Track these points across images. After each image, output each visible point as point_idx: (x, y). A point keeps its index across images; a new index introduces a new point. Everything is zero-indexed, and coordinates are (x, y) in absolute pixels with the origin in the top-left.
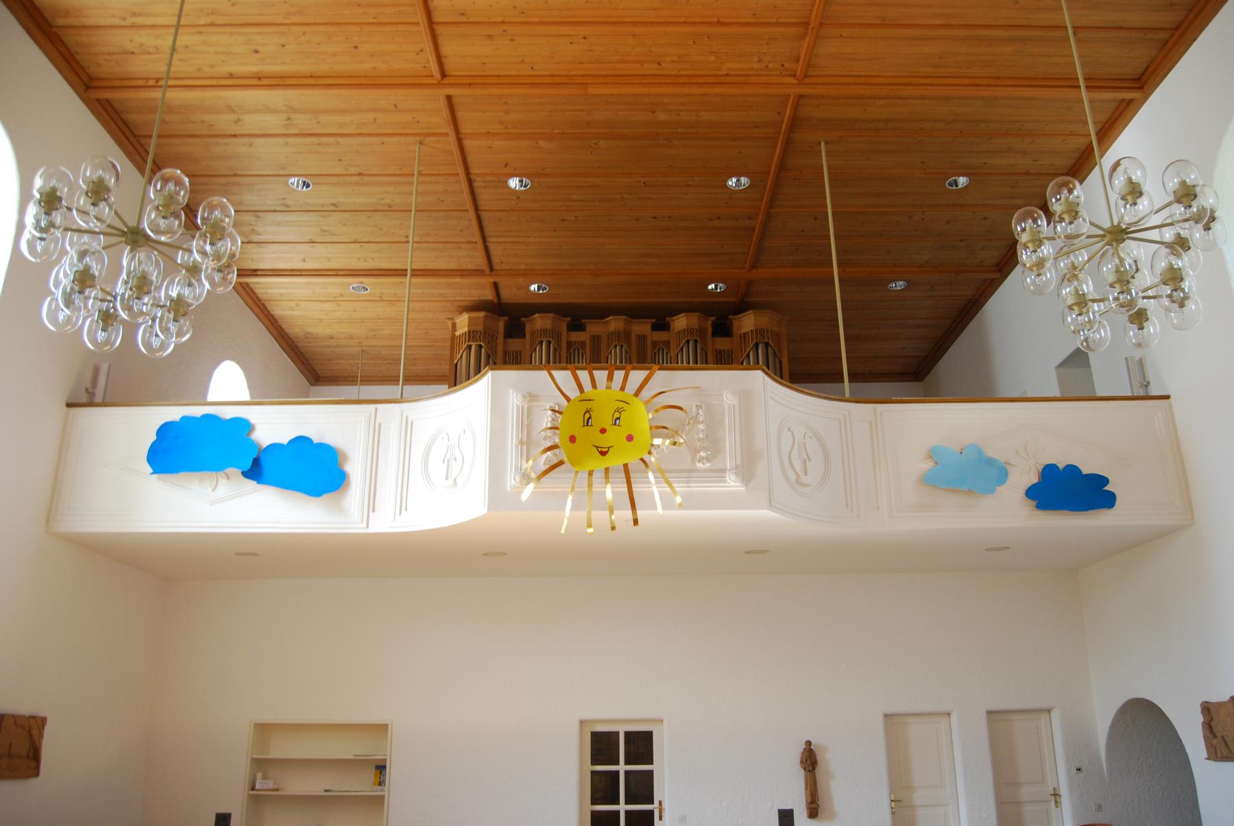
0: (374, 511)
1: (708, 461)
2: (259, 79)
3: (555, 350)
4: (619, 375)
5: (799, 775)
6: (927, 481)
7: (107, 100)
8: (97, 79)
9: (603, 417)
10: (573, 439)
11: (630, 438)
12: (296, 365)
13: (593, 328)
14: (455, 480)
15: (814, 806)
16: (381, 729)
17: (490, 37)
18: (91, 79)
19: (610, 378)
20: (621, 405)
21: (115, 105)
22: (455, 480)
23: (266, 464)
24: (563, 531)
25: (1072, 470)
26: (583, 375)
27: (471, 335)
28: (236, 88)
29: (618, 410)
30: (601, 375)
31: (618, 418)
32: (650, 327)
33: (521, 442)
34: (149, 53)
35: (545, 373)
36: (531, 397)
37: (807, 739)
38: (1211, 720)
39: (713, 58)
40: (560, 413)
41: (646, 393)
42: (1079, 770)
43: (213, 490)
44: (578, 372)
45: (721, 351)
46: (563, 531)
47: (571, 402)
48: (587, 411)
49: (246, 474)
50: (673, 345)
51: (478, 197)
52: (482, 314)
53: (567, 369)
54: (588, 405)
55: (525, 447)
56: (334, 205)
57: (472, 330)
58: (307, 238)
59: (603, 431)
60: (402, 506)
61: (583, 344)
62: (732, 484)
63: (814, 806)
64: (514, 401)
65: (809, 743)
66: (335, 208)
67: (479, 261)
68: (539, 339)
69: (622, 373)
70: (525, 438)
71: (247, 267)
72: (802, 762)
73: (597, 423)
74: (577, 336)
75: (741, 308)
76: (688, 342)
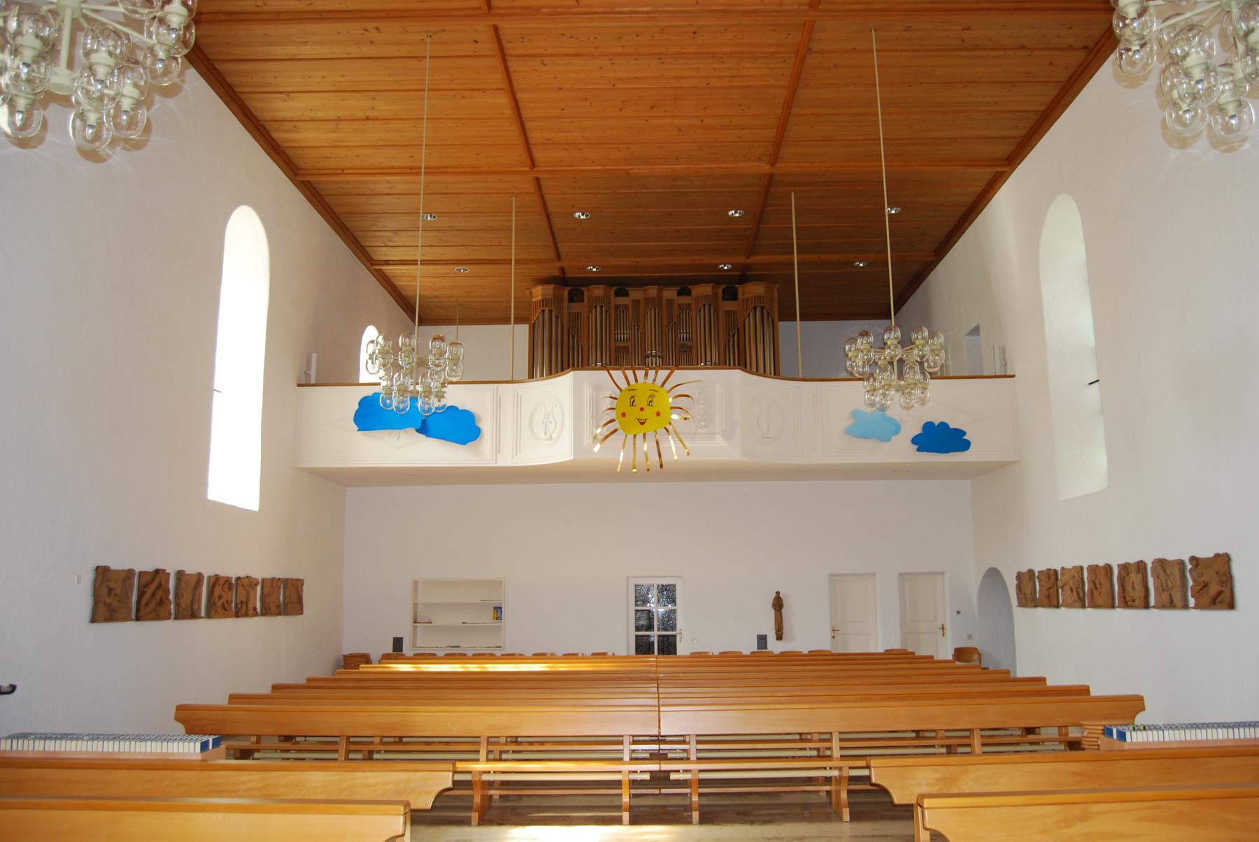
0: (499, 452)
1: (705, 427)
2: (411, 169)
3: (606, 312)
4: (652, 373)
5: (771, 613)
6: (851, 432)
7: (308, 181)
8: (303, 169)
9: (641, 401)
10: (624, 415)
11: (658, 414)
12: (407, 314)
13: (636, 294)
14: (551, 435)
15: (780, 633)
16: (497, 584)
17: (566, 149)
18: (298, 169)
19: (646, 375)
20: (652, 393)
21: (330, 204)
22: (551, 435)
23: (431, 425)
24: (618, 470)
25: (944, 425)
26: (630, 373)
27: (544, 302)
28: (762, 760)
29: (652, 396)
30: (640, 373)
31: (651, 401)
32: (676, 293)
33: (592, 417)
34: (341, 158)
35: (606, 372)
36: (597, 388)
37: (1031, 568)
38: (1020, 583)
39: (713, 156)
40: (615, 399)
41: (668, 386)
42: (958, 612)
43: (397, 440)
44: (627, 372)
45: (728, 311)
46: (618, 470)
47: (623, 392)
48: (632, 397)
49: (418, 431)
50: (693, 307)
51: (515, 83)
52: (552, 286)
53: (619, 369)
54: (633, 393)
55: (595, 420)
56: (450, 227)
57: (544, 298)
58: (429, 244)
59: (642, 409)
60: (517, 449)
61: (626, 307)
62: (720, 442)
63: (780, 633)
64: (587, 390)
65: (778, 593)
66: (451, 229)
67: (551, 253)
68: (595, 304)
69: (654, 371)
70: (595, 414)
71: (381, 259)
72: (773, 605)
73: (638, 404)
74: (622, 301)
75: (743, 279)
76: (704, 305)
